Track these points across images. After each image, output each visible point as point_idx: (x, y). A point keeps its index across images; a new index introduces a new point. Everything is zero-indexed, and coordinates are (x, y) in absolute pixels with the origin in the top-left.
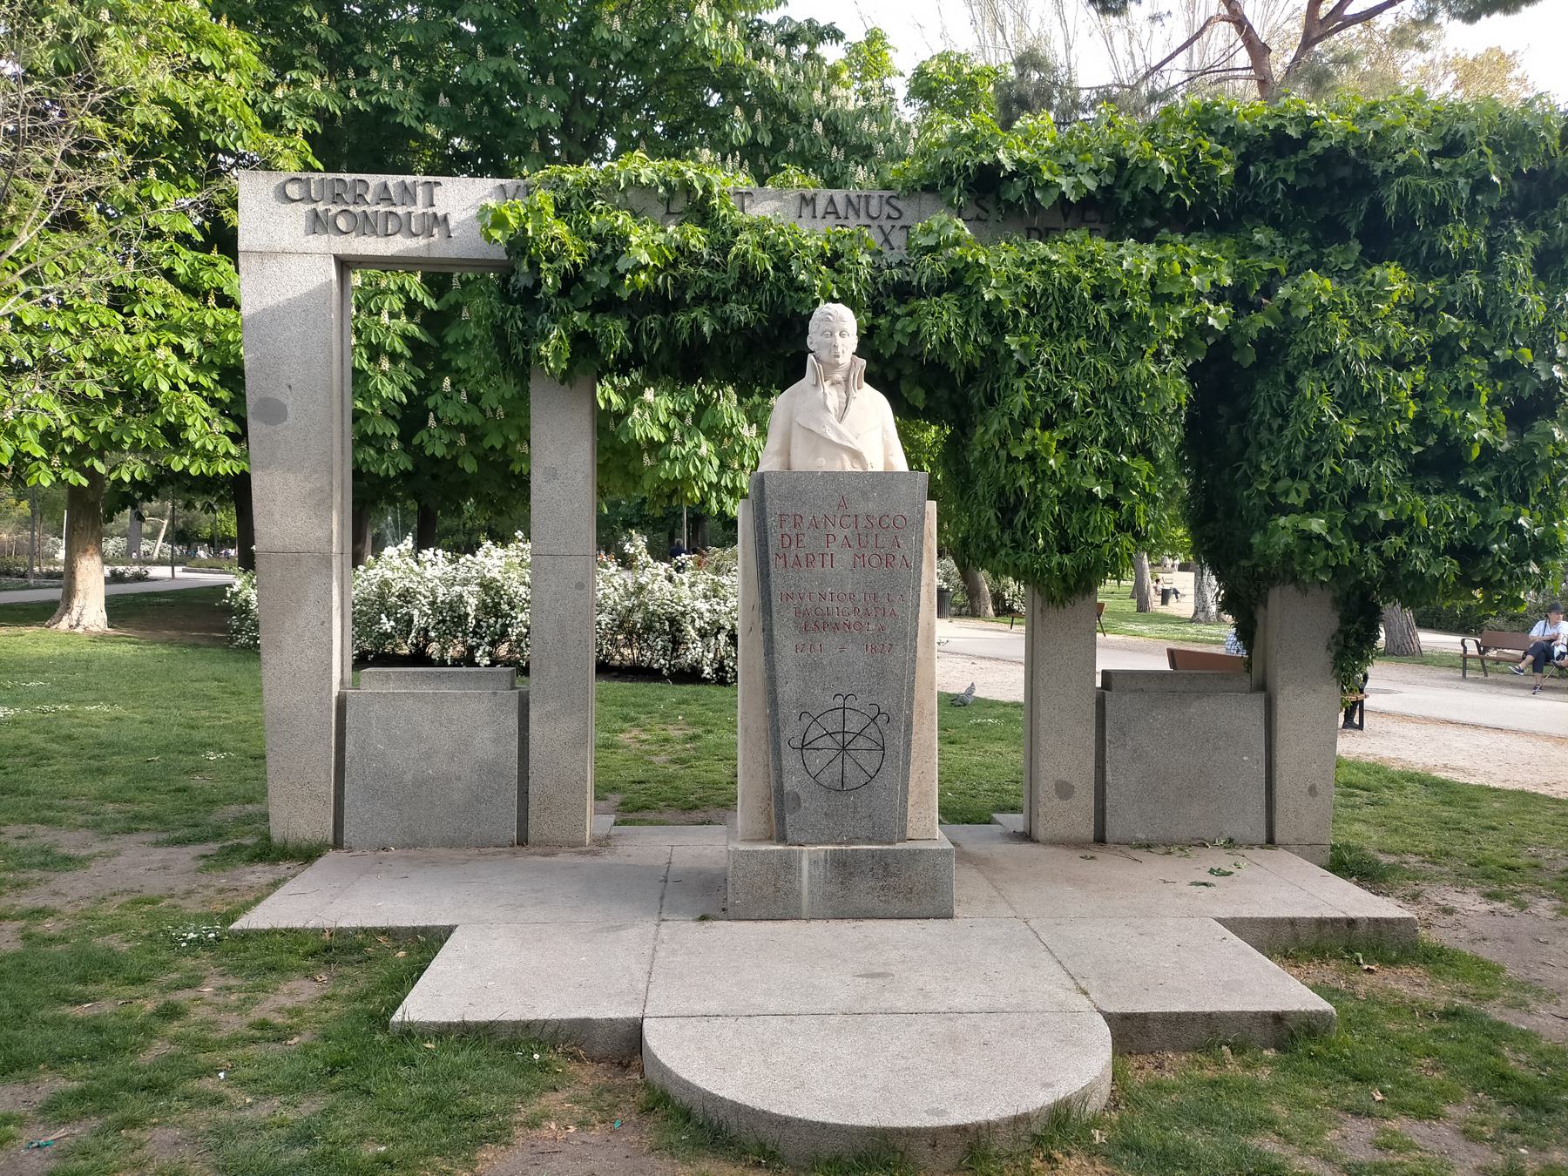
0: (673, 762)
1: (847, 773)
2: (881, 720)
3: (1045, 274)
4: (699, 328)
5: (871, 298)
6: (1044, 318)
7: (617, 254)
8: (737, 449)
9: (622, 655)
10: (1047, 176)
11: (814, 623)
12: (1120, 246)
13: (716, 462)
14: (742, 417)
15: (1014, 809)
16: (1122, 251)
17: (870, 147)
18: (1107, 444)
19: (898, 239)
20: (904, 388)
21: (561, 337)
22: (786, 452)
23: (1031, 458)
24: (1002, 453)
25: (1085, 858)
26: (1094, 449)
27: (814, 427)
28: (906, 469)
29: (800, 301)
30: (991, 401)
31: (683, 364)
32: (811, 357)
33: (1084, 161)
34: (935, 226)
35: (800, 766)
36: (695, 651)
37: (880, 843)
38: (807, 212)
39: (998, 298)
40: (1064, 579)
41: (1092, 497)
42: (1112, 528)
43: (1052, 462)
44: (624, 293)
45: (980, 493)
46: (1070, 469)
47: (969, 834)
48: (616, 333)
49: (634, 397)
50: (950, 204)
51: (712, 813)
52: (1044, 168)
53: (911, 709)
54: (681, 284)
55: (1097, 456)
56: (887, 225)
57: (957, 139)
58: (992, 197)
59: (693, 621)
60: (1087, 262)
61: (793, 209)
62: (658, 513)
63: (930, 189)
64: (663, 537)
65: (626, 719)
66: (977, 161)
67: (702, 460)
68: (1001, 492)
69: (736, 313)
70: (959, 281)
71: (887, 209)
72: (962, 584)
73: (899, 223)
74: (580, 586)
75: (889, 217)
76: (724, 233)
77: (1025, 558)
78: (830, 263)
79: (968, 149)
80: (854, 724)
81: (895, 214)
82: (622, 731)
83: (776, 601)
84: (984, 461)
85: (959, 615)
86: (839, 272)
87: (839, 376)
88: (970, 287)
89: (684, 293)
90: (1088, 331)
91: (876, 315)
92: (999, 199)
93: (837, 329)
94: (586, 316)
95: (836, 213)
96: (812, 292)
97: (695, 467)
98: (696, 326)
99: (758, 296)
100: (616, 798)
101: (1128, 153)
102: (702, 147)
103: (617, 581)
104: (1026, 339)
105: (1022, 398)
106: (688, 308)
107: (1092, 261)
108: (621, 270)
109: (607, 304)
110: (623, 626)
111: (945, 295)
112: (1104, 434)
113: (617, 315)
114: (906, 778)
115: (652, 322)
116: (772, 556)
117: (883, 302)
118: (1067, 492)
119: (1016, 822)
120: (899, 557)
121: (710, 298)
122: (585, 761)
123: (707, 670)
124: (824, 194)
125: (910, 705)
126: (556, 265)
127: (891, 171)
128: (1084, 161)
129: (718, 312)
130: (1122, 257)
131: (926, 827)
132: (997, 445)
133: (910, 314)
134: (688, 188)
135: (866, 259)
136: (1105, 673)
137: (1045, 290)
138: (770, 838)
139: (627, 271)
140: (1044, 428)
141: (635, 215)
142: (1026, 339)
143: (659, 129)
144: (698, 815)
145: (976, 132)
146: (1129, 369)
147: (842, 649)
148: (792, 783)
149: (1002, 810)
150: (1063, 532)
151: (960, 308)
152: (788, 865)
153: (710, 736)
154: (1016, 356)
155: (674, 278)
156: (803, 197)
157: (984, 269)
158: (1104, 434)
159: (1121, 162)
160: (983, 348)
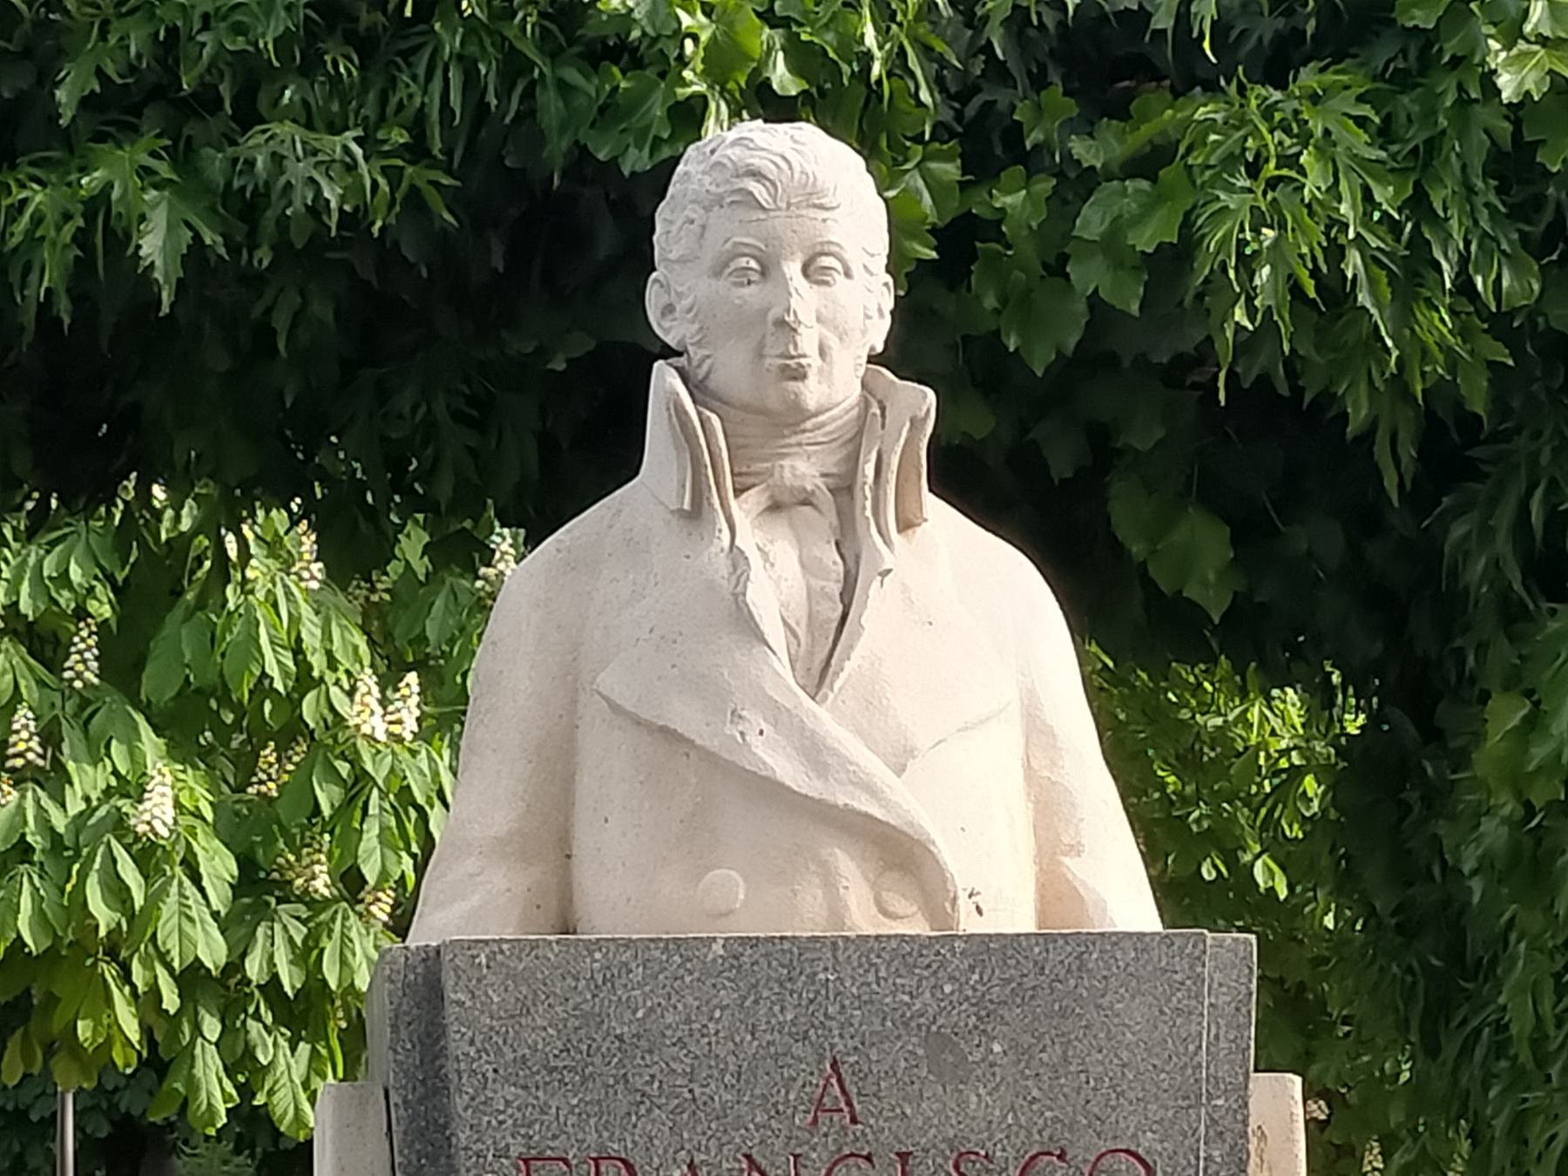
4: (120, 241)
5: (956, 91)
13: (219, 865)
14: (351, 641)
20: (1127, 515)
22: (551, 841)
27: (686, 717)
29: (610, 112)
32: (665, 379)
45: (1521, 1026)
67: (148, 856)
69: (298, 170)
87: (804, 468)
88: (1427, 40)
89: (47, 79)
97: (117, 892)
98: (105, 232)
99: (408, 90)
106: (69, 148)
111: (1308, 78)
129: (215, 163)
151: (1385, 134)
160: (1500, 323)
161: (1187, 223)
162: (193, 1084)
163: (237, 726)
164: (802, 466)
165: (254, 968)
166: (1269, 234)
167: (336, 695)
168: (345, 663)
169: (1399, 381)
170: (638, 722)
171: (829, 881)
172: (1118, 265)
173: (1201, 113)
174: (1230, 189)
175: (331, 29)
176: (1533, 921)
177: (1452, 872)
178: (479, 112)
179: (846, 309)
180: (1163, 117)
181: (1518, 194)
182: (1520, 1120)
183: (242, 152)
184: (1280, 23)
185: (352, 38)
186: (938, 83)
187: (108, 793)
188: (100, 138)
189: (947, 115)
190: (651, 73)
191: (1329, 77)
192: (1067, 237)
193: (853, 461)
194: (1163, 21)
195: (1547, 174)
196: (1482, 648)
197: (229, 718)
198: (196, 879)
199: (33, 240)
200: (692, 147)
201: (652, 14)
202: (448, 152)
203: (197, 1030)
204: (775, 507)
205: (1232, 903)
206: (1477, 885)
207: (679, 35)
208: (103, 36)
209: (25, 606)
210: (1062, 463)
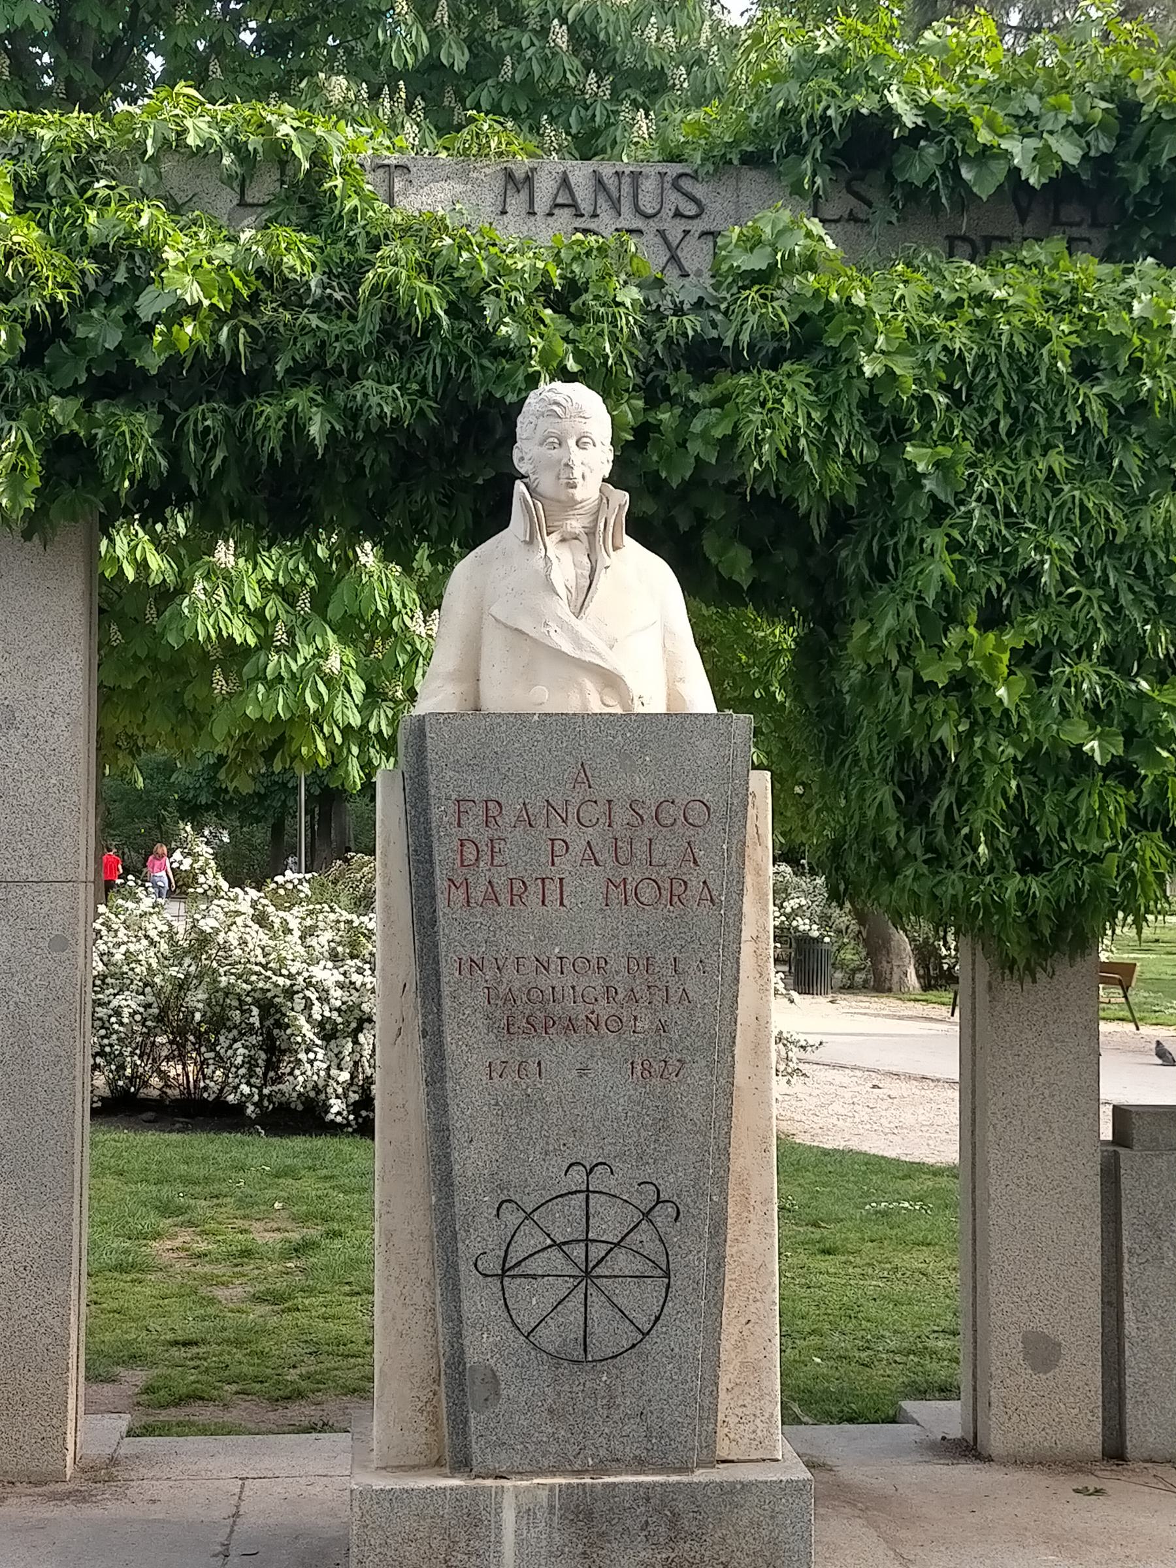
0: (258, 1299)
1: (596, 1328)
2: (663, 1215)
3: (978, 325)
4: (302, 429)
5: (643, 371)
6: (982, 412)
7: (137, 284)
8: (402, 659)
9: (163, 1075)
10: (984, 136)
11: (527, 1018)
12: (1130, 271)
13: (358, 686)
14: (412, 596)
15: (946, 1391)
16: (1132, 281)
17: (660, 73)
18: (1110, 656)
19: (696, 256)
20: (710, 545)
21: (24, 446)
22: (471, 674)
23: (961, 684)
24: (905, 675)
25: (1084, 1491)
26: (1084, 666)
27: (526, 625)
28: (712, 708)
29: (501, 377)
30: (880, 572)
31: (279, 499)
32: (520, 487)
33: (1056, 109)
34: (768, 232)
35: (497, 1310)
36: (311, 1068)
37: (664, 1469)
38: (517, 203)
39: (890, 372)
40: (1032, 923)
41: (1082, 761)
42: (1122, 822)
43: (1001, 692)
44: (152, 360)
45: (864, 753)
46: (1034, 701)
47: (849, 1447)
48: (135, 437)
49: (195, 558)
50: (797, 189)
51: (332, 1407)
52: (977, 121)
53: (724, 1192)
54: (266, 343)
55: (1091, 681)
56: (675, 231)
57: (811, 65)
58: (878, 176)
59: (309, 1006)
60: (1060, 303)
61: (489, 199)
62: (246, 786)
63: (757, 160)
64: (261, 834)
65: (165, 1209)
66: (847, 106)
67: (329, 681)
68: (904, 752)
69: (374, 400)
70: (814, 339)
71: (674, 199)
72: (854, 927)
73: (697, 227)
74: (60, 944)
75: (678, 214)
76: (351, 243)
77: (953, 884)
78: (560, 304)
79: (829, 84)
80: (609, 1222)
81: (690, 209)
82: (157, 1235)
83: (449, 975)
84: (868, 690)
85: (849, 988)
86: (578, 319)
87: (575, 525)
88: (835, 351)
89: (272, 361)
90: (1068, 437)
91: (652, 404)
92: (890, 179)
93: (572, 432)
94: (74, 405)
95: (574, 205)
96: (526, 360)
97: (317, 696)
98: (295, 425)
99: (419, 367)
100: (135, 1378)
101: (1142, 93)
102: (332, 72)
103: (155, 926)
104: (946, 452)
105: (941, 568)
106: (279, 389)
107: (1073, 301)
108: (145, 314)
109: (117, 381)
110: (169, 1019)
111: (787, 367)
112: (1104, 637)
113: (137, 404)
114: (715, 1333)
115: (209, 416)
116: (441, 883)
117: (667, 379)
118: (1034, 752)
119: (944, 1417)
120: (695, 884)
121: (323, 371)
122: (64, 1303)
123: (337, 1105)
124: (552, 166)
125: (722, 1183)
126: (14, 305)
127: (685, 123)
128: (1056, 109)
129: (340, 397)
130: (1132, 293)
131: (756, 1436)
132: (894, 658)
133: (719, 402)
134: (281, 154)
135: (630, 295)
136: (1121, 1114)
137: (982, 357)
138: (438, 1463)
139: (158, 317)
140: (985, 625)
141: (175, 209)
142: (946, 452)
143: (247, 38)
144: (299, 1412)
145: (845, 51)
146: (1147, 512)
147: (583, 1071)
148: (480, 1348)
149: (921, 1393)
150: (1028, 830)
151: (817, 391)
152: (474, 1519)
153: (337, 1243)
154: (929, 485)
155: (251, 330)
156: (509, 176)
157: (862, 316)
158: (1104, 637)
159: (1128, 111)
160: (862, 469)
161: (735, 426)
162: (347, 773)
163: (366, 631)
164: (574, 523)
165: (372, 727)
166: (769, 431)
167: (406, 618)
168: (410, 605)
169: (820, 492)
170: (506, 626)
171: (582, 691)
172: (707, 443)
173: (742, 381)
174: (753, 412)
175: (388, 343)
176: (870, 712)
177: (839, 692)
178: (448, 377)
179: (595, 460)
180: (727, 382)
181: (871, 416)
182: (862, 792)
183: (352, 392)
184: (776, 344)
185: (396, 346)
186: (636, 367)
187: (314, 656)
188: (293, 385)
189: (639, 381)
190: (518, 362)
191: (795, 367)
192: (687, 432)
193: (596, 520)
194: (728, 343)
195: (883, 408)
196: (852, 602)
197: (363, 627)
198: (349, 692)
199: (266, 427)
200: (532, 394)
201: (519, 337)
202: (436, 394)
203: (349, 751)
204: (563, 540)
205: (742, 704)
206: (848, 697)
207: (530, 346)
208: (295, 344)
209: (281, 580)
210: (684, 526)
